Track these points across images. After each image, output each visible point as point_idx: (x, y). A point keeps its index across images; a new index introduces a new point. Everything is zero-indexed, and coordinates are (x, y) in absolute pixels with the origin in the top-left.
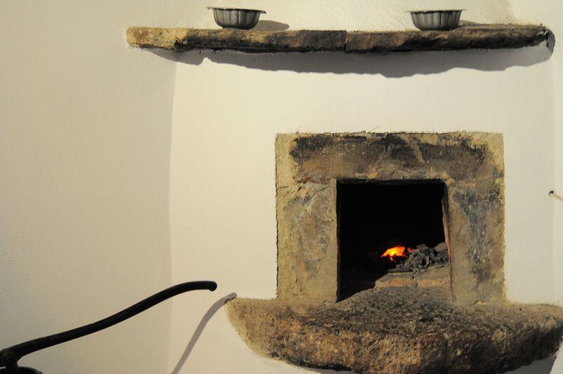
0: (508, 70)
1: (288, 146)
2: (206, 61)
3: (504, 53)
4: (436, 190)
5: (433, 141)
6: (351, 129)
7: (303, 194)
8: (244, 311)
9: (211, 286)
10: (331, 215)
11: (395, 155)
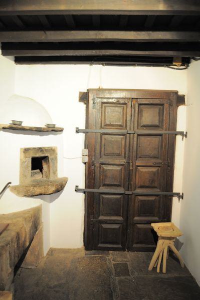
1: (23, 150)
6: (34, 147)
11: (41, 151)
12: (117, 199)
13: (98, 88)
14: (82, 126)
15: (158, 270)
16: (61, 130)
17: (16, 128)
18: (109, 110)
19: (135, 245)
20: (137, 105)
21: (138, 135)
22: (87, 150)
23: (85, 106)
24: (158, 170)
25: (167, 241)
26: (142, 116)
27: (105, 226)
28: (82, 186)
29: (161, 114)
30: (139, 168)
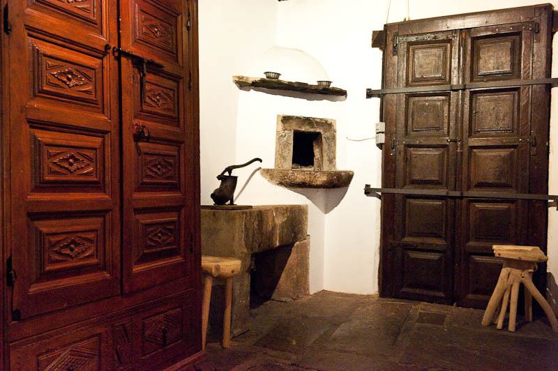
1: (280, 119)
4: (319, 134)
5: (318, 120)
7: (284, 134)
8: (267, 172)
11: (309, 124)
12: (435, 208)
13: (402, 20)
14: (377, 86)
15: (500, 324)
16: (342, 93)
17: (271, 85)
18: (420, 55)
19: (470, 296)
20: (469, 41)
21: (473, 93)
22: (384, 123)
23: (382, 53)
24: (512, 153)
25: (516, 272)
26: (479, 58)
27: (413, 255)
28: (376, 183)
29: (515, 52)
30: (475, 150)
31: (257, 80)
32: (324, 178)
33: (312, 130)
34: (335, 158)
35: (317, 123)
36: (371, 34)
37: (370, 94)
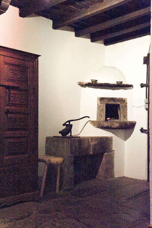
0: (128, 90)
1: (99, 99)
2: (87, 87)
3: (126, 88)
4: (119, 105)
7: (101, 105)
8: (93, 122)
9: (89, 117)
10: (105, 109)
17: (94, 85)
31: (87, 83)
32: (118, 125)
33: (115, 103)
34: (127, 115)
35: (117, 100)
36: (143, 58)
37: (142, 86)
